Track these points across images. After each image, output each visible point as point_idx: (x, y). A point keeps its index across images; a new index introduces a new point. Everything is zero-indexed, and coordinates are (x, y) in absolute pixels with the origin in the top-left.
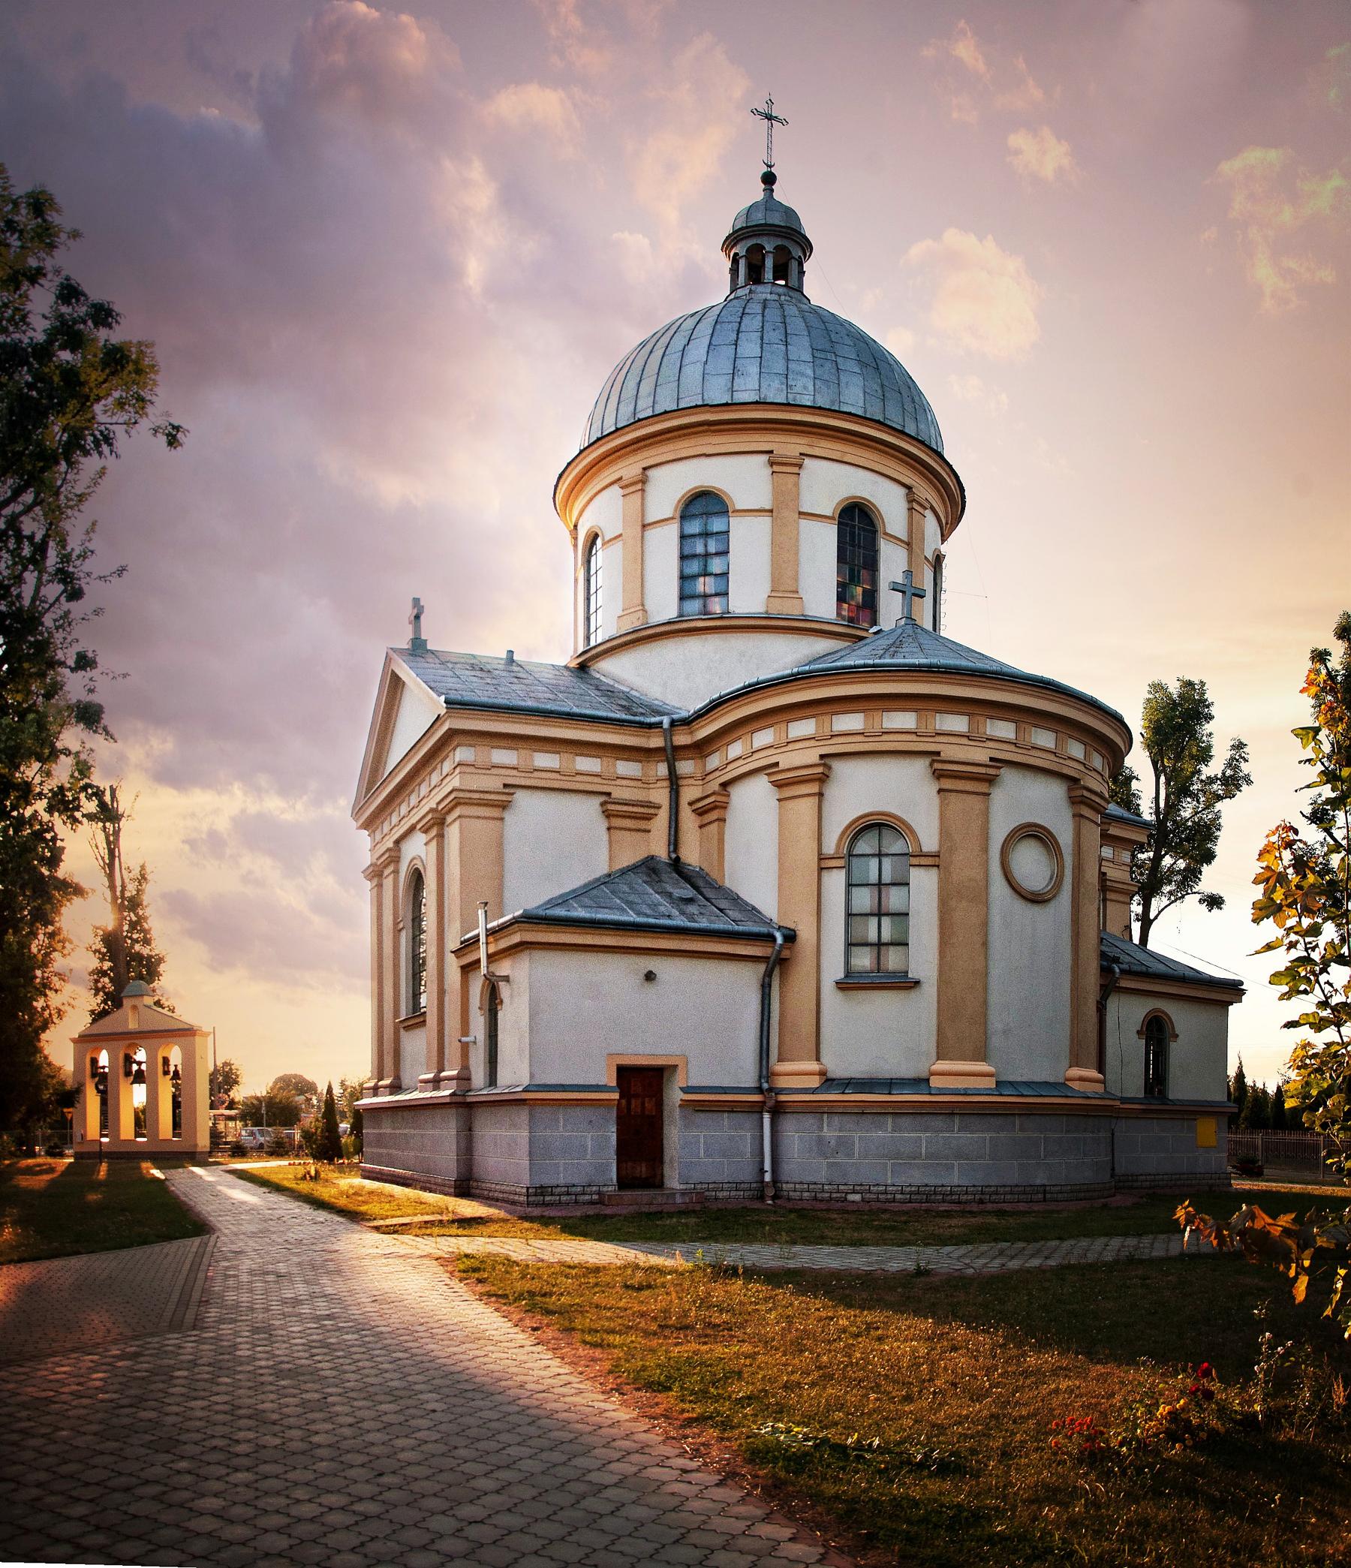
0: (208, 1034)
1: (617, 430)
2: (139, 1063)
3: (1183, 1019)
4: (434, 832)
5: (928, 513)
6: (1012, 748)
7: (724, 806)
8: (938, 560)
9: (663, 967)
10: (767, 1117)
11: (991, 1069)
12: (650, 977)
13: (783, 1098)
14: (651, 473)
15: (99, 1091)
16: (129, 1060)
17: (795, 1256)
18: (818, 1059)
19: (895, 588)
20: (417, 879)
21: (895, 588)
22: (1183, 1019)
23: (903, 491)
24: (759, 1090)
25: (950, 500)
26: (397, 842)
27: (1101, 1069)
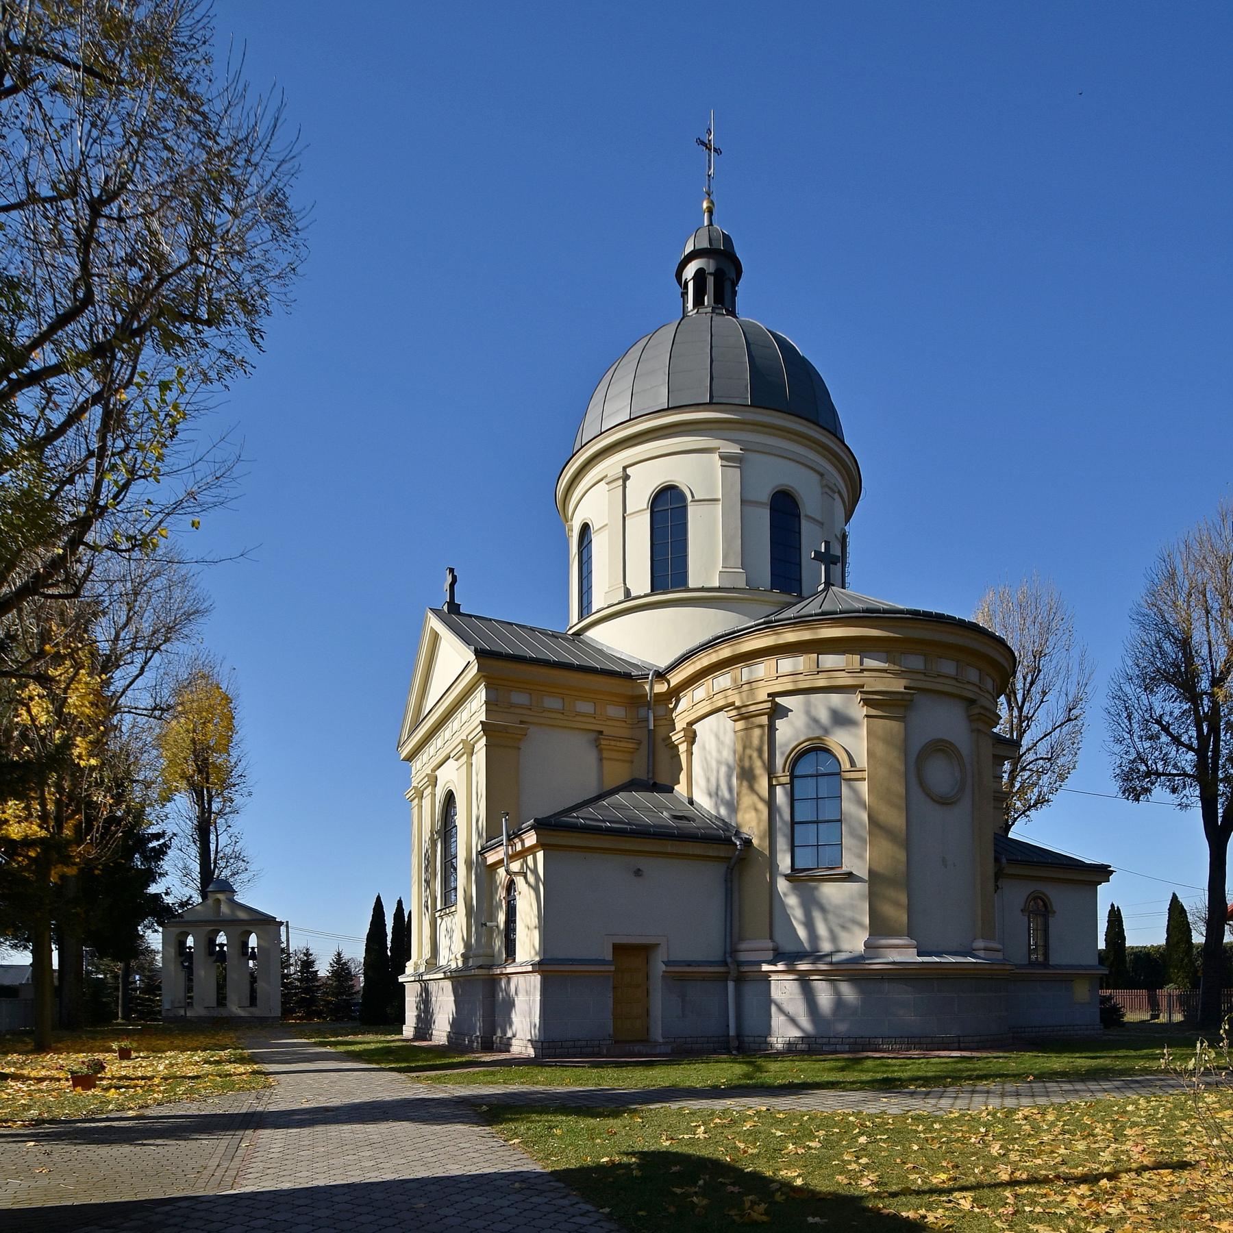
0: (282, 923)
1: (668, 409)
2: (221, 945)
3: (1060, 898)
5: (836, 496)
6: (922, 677)
8: (844, 537)
9: (641, 862)
10: (731, 985)
11: (1000, 947)
12: (638, 873)
13: (746, 969)
14: (629, 471)
15: (184, 967)
16: (212, 942)
17: (624, 1080)
18: (771, 938)
19: (819, 557)
20: (450, 798)
21: (819, 557)
22: (1060, 898)
23: (816, 477)
24: (724, 963)
25: (851, 485)
26: (434, 770)
27: (771, 938)
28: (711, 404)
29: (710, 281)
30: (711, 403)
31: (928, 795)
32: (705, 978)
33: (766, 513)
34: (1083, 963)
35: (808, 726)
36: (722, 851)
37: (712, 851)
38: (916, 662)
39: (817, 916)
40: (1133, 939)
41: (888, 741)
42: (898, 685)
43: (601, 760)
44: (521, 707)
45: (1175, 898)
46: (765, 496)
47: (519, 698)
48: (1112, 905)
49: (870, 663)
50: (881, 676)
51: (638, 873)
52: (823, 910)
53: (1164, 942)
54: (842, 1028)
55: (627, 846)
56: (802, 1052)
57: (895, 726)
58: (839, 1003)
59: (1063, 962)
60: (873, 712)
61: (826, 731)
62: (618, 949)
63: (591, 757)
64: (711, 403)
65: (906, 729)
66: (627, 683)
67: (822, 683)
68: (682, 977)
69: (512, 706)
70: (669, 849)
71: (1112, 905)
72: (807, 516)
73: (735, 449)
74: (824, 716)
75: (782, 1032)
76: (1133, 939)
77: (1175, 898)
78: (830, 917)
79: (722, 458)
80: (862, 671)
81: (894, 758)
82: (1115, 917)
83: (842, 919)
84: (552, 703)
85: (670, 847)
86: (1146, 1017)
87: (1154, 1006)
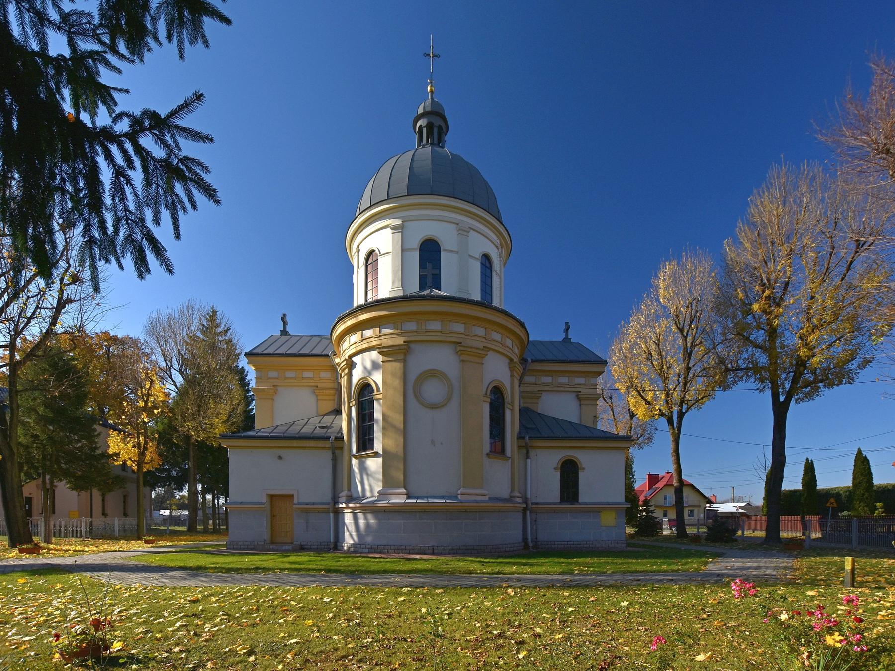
4: (402, 357)
7: (538, 398)
10: (331, 515)
23: (454, 226)
28: (389, 199)
29: (424, 130)
30: (388, 198)
31: (422, 404)
32: (319, 512)
33: (417, 254)
34: (610, 500)
35: (363, 372)
36: (327, 444)
37: (321, 444)
38: (411, 326)
39: (365, 477)
40: (822, 483)
41: (393, 375)
42: (400, 341)
43: (317, 400)
44: (291, 378)
45: (859, 452)
46: (415, 243)
47: (272, 374)
48: (807, 459)
49: (385, 331)
50: (389, 337)
51: (280, 458)
52: (368, 475)
53: (850, 484)
54: (369, 539)
55: (544, 444)
56: (352, 552)
57: (397, 366)
58: (368, 526)
59: (587, 500)
60: (386, 359)
61: (370, 373)
62: (272, 497)
63: (313, 399)
64: (388, 198)
65: (405, 367)
66: (325, 359)
67: (365, 346)
68: (307, 511)
69: (269, 378)
70: (295, 445)
71: (807, 459)
72: (445, 250)
73: (398, 222)
74: (369, 365)
75: (349, 541)
76: (822, 483)
77: (859, 452)
78: (371, 478)
79: (392, 229)
80: (380, 336)
81: (397, 383)
82: (809, 468)
83: (370, 475)
84: (290, 374)
85: (295, 443)
86: (799, 534)
87: (805, 528)
